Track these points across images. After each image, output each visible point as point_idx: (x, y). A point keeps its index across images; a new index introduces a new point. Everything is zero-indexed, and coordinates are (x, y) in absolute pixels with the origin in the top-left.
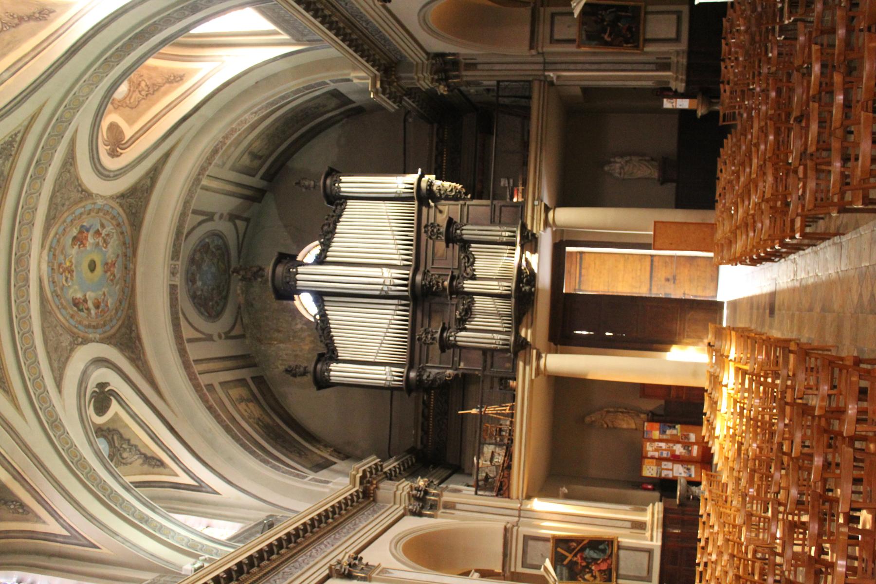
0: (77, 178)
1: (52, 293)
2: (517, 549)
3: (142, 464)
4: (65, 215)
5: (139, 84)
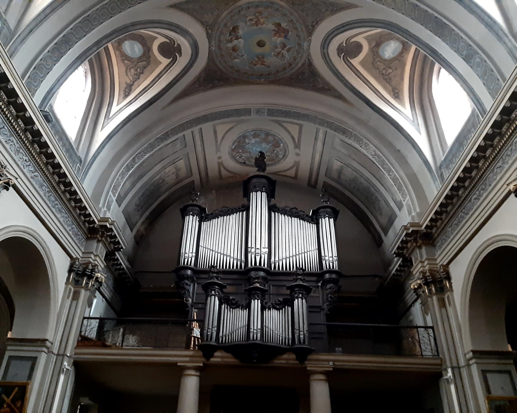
0: (322, 20)
1: (240, 6)
2: (26, 351)
3: (126, 83)
4: (296, 14)
5: (390, 68)
